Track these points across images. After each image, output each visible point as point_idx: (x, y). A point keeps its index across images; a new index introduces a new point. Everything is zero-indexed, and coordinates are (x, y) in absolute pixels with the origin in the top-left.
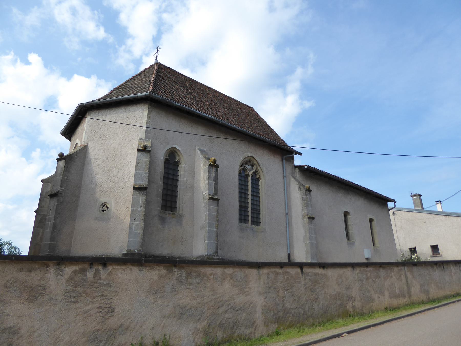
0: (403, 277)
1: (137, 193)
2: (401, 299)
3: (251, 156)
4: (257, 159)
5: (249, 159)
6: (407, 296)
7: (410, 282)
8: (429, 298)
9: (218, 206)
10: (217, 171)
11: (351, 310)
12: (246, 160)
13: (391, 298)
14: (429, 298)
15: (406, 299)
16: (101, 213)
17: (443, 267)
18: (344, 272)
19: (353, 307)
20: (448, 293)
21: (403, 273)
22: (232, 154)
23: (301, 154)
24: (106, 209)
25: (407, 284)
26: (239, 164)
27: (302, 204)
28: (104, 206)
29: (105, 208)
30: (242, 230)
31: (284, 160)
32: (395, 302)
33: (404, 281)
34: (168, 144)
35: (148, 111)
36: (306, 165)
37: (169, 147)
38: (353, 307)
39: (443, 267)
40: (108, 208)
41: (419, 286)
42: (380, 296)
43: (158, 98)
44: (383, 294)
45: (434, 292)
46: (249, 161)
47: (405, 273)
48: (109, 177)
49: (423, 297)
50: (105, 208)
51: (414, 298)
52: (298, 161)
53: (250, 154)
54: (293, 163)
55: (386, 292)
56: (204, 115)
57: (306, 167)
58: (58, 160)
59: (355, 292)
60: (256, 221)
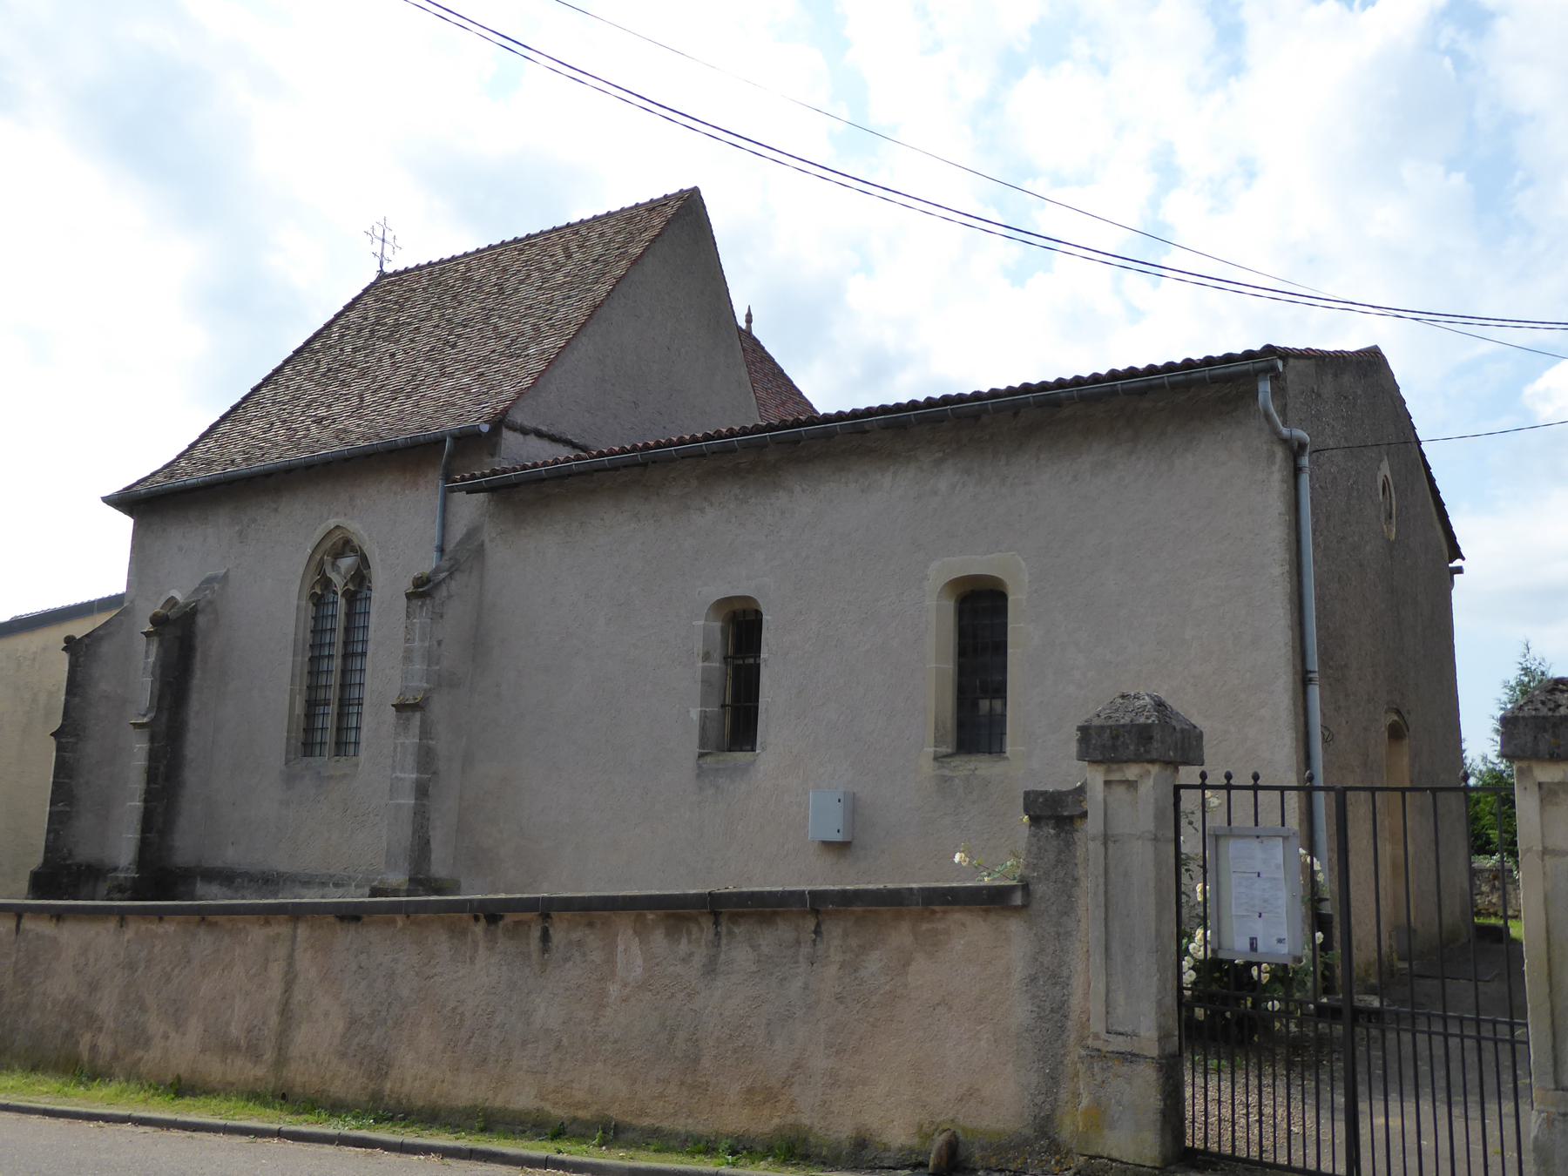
0: (276, 971)
2: (239, 1063)
5: (337, 536)
6: (269, 1056)
7: (299, 996)
8: (376, 1097)
11: (85, 1055)
12: (328, 544)
13: (203, 1051)
14: (376, 1097)
15: (260, 1071)
17: (545, 937)
18: (98, 934)
19: (93, 1048)
20: (523, 1099)
21: (281, 951)
25: (285, 1011)
30: (290, 779)
32: (215, 1069)
33: (275, 990)
38: (93, 1048)
39: (545, 937)
41: (340, 1026)
42: (172, 1035)
44: (179, 1026)
45: (417, 1071)
47: (291, 957)
49: (346, 1080)
51: (299, 1075)
53: (332, 523)
55: (193, 1021)
58: (409, 596)
59: (106, 1006)
60: (343, 746)
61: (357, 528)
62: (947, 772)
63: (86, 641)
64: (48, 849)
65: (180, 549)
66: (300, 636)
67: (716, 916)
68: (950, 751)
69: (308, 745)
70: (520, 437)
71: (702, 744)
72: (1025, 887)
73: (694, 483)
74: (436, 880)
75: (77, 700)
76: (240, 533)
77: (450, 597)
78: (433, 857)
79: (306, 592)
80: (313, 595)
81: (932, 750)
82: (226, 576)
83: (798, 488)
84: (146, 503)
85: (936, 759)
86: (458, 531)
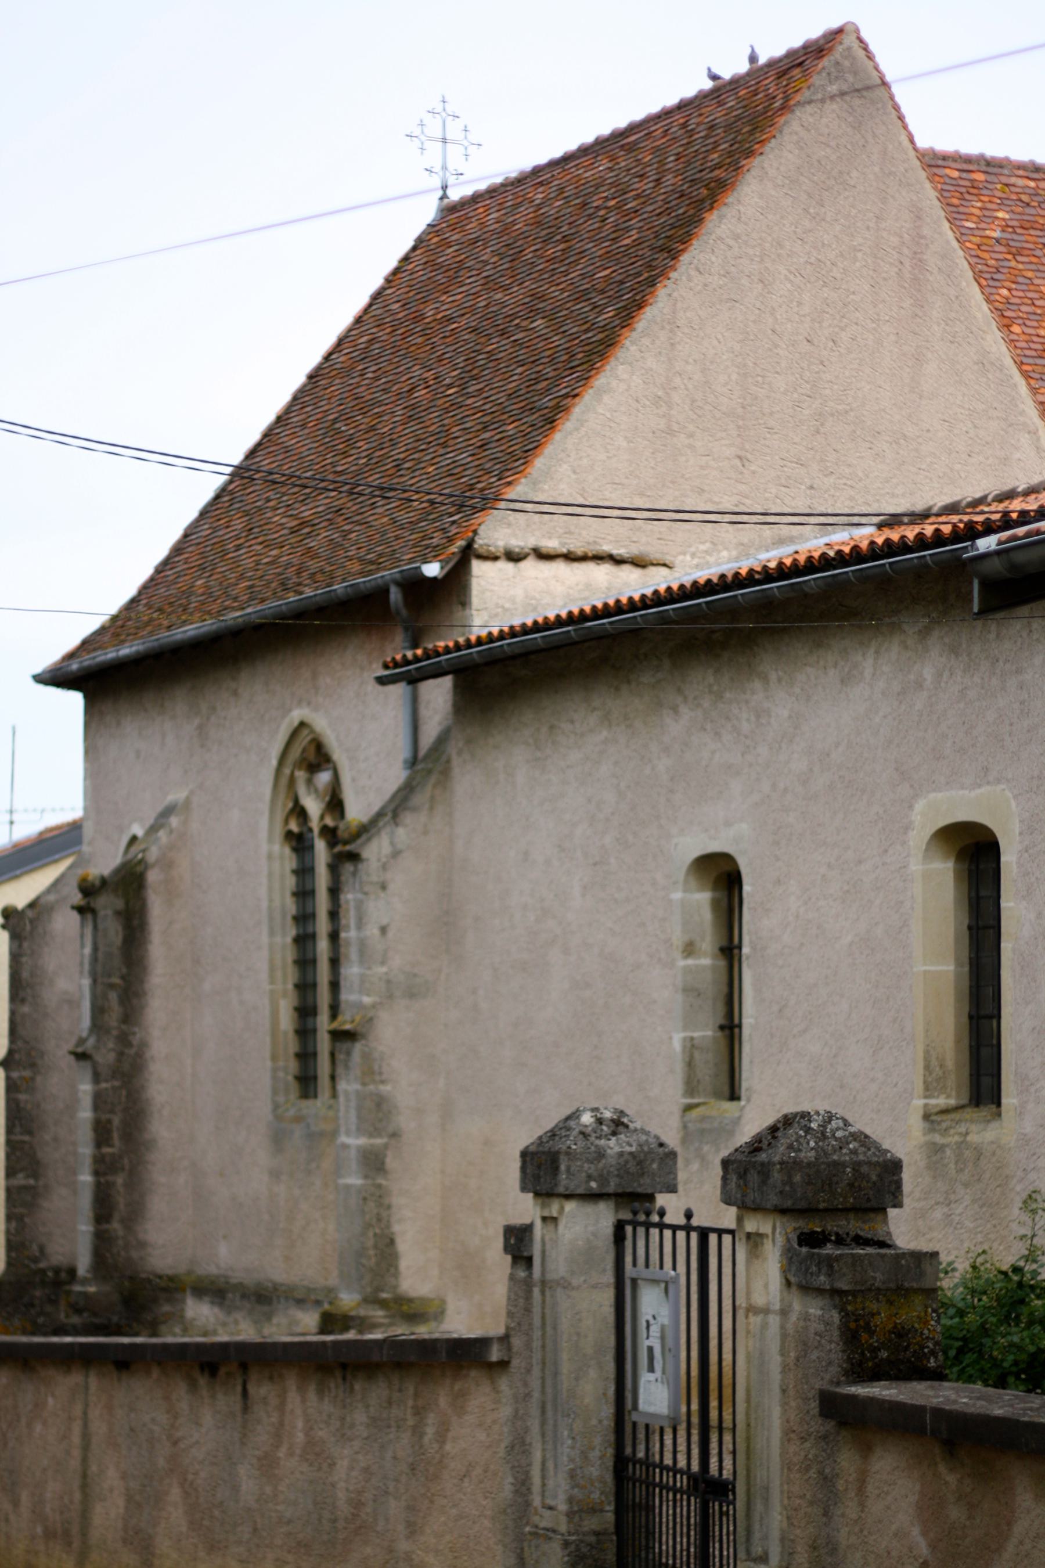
12: (296, 753)
61: (321, 724)
62: (938, 1138)
63: (30, 913)
64: (10, 1246)
65: (138, 753)
66: (277, 903)
67: (244, 1367)
68: (952, 1102)
69: (306, 1083)
70: (508, 567)
71: (691, 1088)
72: (505, 1339)
73: (667, 663)
74: (410, 1300)
75: (26, 1009)
76: (200, 727)
77: (396, 854)
78: (403, 1264)
79: (279, 831)
80: (289, 835)
81: (919, 1103)
82: (187, 802)
83: (773, 676)
84: (109, 678)
85: (927, 1117)
86: (430, 732)
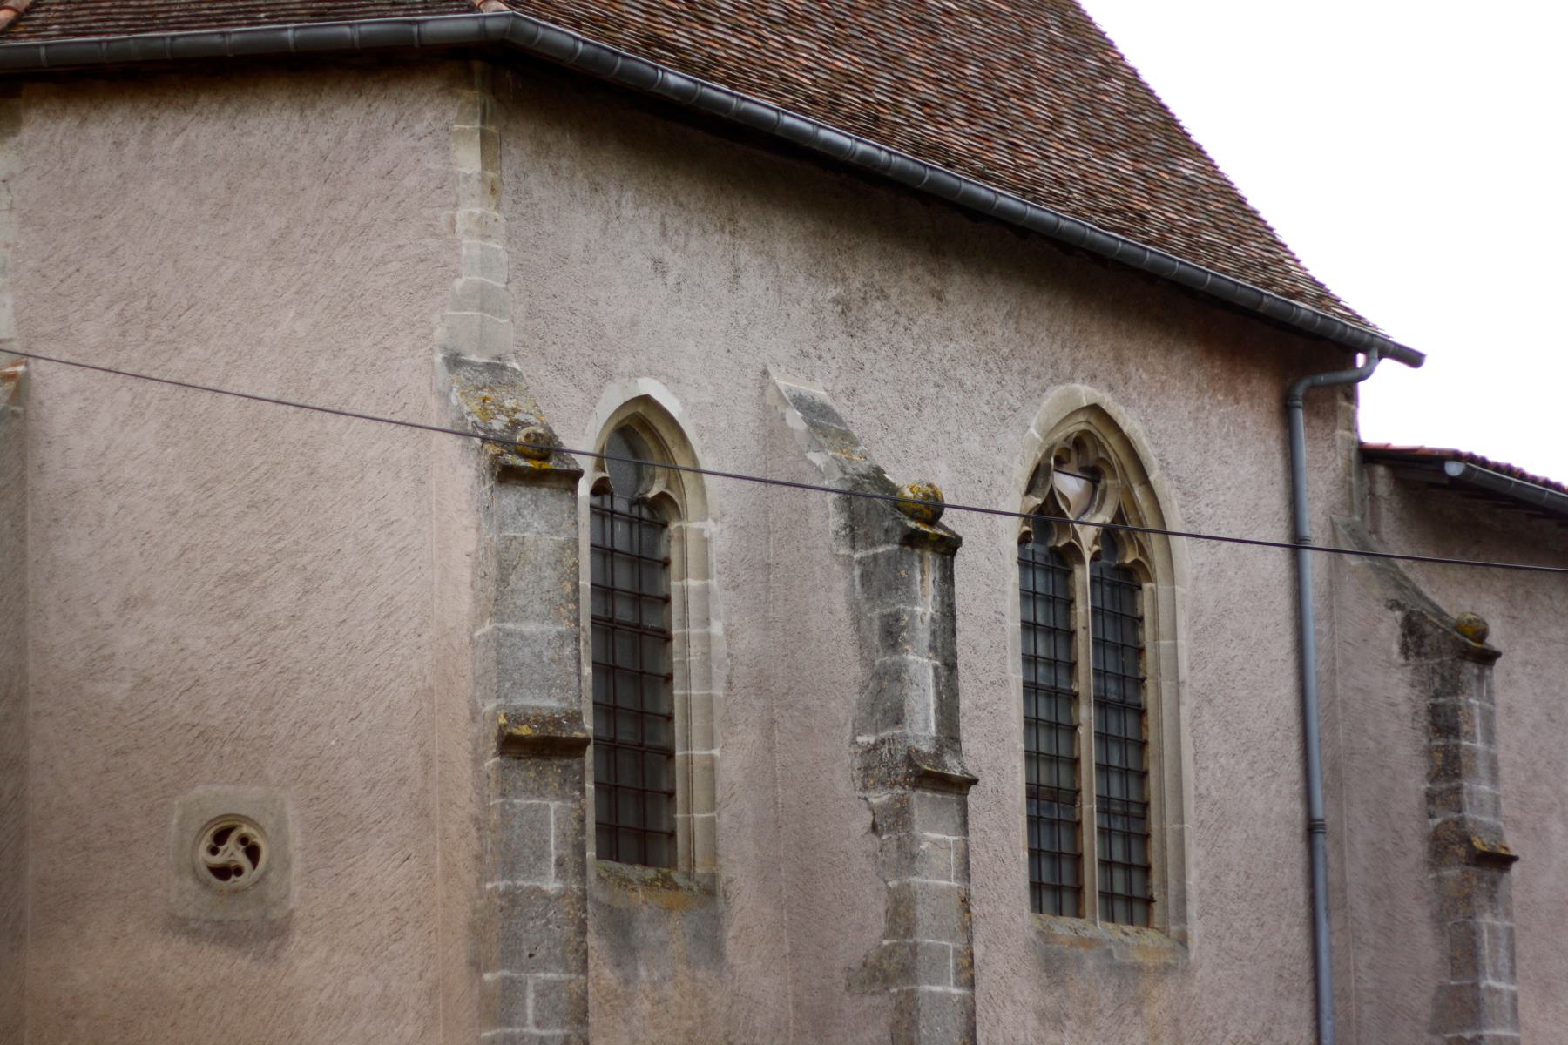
1: (525, 773)
3: (1095, 409)
4: (1130, 422)
5: (1077, 426)
9: (964, 825)
10: (947, 578)
12: (1059, 436)
16: (207, 885)
22: (971, 394)
23: (1412, 359)
24: (241, 859)
26: (1021, 473)
27: (1429, 752)
28: (221, 837)
29: (231, 852)
31: (1300, 415)
34: (609, 377)
35: (485, 137)
36: (1456, 456)
37: (613, 398)
40: (253, 852)
43: (559, 48)
46: (1091, 449)
48: (236, 628)
50: (231, 852)
52: (1389, 411)
53: (1086, 393)
54: (1352, 426)
56: (827, 144)
57: (1454, 469)
